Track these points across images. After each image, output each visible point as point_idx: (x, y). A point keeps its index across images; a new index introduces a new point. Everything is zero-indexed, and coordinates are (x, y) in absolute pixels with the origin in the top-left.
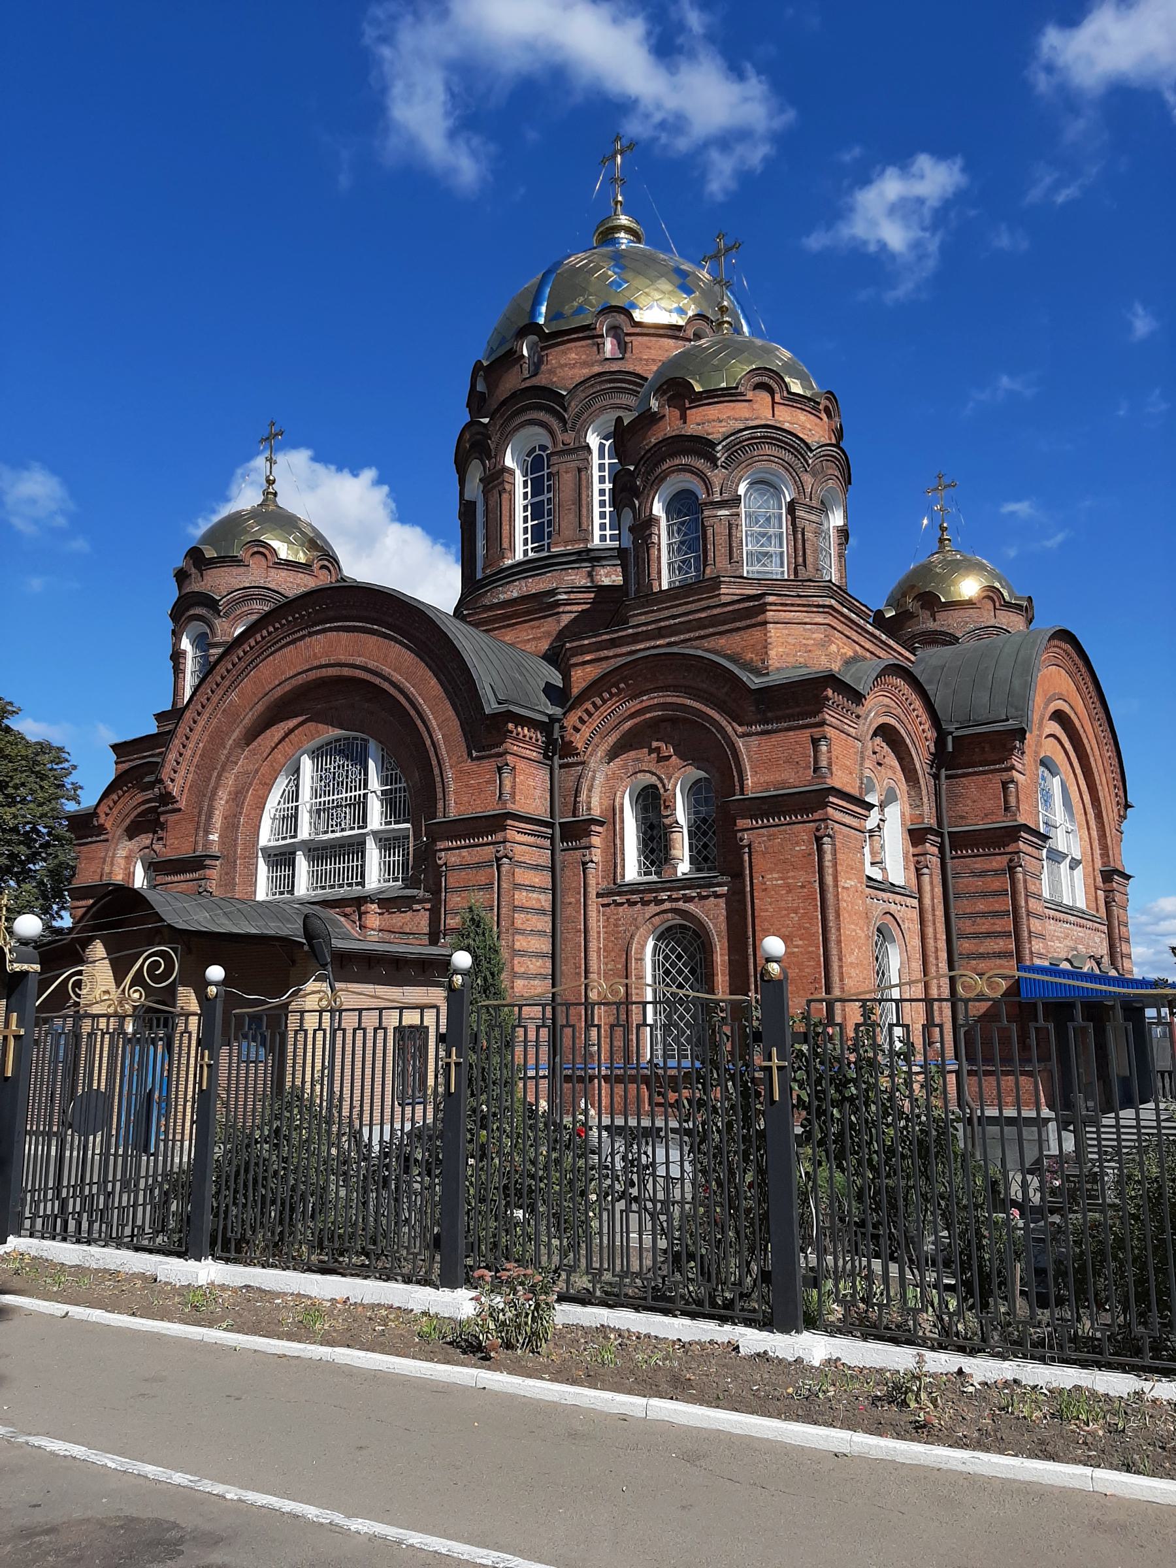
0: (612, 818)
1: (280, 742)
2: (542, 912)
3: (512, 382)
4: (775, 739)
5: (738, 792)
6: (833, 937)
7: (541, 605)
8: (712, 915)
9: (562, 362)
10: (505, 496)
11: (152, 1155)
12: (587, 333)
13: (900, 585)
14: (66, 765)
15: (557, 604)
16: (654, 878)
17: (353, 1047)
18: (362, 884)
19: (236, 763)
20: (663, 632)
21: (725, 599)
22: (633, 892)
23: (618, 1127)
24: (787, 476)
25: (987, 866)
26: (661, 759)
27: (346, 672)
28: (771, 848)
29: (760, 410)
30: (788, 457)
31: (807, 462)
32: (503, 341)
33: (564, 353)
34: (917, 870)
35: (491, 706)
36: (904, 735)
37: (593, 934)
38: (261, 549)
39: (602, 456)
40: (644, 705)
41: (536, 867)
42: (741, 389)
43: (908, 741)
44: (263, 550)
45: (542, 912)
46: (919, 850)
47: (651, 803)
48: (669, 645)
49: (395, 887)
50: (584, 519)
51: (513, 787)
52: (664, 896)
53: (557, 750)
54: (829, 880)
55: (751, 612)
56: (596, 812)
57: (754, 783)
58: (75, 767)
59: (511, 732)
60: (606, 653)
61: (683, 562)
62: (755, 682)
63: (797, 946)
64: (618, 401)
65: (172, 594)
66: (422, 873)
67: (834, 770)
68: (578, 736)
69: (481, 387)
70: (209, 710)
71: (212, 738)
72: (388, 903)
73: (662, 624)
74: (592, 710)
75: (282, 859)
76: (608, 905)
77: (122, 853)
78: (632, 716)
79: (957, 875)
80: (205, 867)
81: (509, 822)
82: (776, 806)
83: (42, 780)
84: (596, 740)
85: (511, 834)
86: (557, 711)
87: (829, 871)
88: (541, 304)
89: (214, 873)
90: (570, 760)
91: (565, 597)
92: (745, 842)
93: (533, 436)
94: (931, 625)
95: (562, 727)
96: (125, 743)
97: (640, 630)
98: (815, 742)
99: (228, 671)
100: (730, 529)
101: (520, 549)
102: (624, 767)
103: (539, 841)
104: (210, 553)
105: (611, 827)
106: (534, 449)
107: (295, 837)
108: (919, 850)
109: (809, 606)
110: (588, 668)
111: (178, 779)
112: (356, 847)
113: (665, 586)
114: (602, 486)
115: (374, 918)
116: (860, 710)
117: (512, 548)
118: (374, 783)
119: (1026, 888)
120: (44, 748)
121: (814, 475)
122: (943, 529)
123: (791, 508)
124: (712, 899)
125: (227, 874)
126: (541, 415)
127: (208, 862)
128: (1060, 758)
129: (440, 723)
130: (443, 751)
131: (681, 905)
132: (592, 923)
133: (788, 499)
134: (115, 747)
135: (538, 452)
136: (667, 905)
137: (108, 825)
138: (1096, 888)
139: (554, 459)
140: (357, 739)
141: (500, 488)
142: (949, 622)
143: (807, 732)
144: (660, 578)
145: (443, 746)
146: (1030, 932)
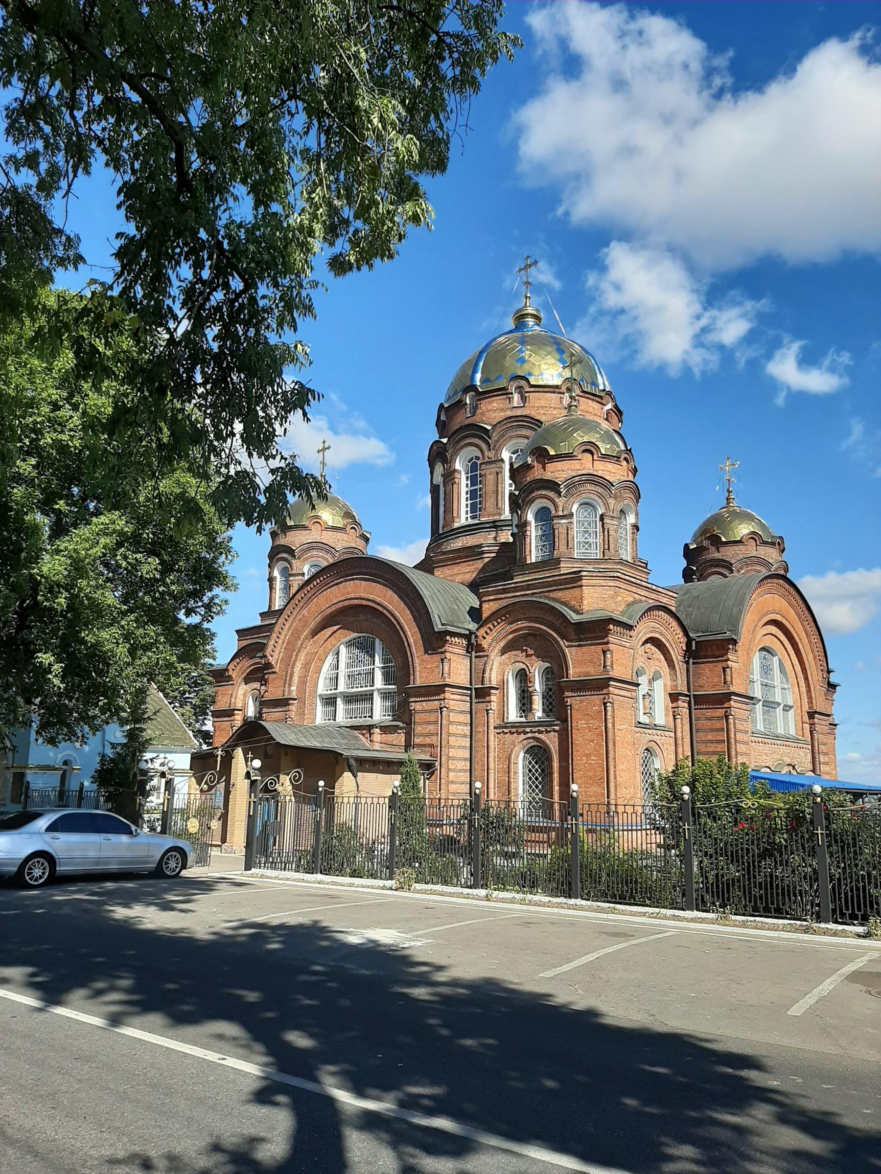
0: (502, 687)
2: (465, 736)
4: (585, 649)
6: (611, 756)
7: (473, 552)
8: (552, 740)
10: (455, 486)
12: (503, 391)
13: (700, 528)
15: (483, 553)
16: (523, 720)
17: (365, 799)
18: (371, 717)
21: (562, 572)
22: (513, 727)
24: (600, 501)
26: (527, 656)
27: (364, 602)
28: (581, 706)
29: (585, 464)
30: (600, 490)
32: (456, 393)
33: (490, 403)
34: (674, 716)
35: (438, 627)
36: (665, 642)
37: (492, 749)
41: (461, 712)
43: (667, 645)
44: (317, 520)
45: (465, 736)
46: (675, 705)
47: (523, 677)
49: (387, 720)
50: (499, 502)
51: (449, 670)
52: (528, 730)
53: (474, 648)
54: (610, 725)
55: (575, 580)
56: (494, 683)
57: (574, 672)
61: (543, 546)
62: (574, 617)
66: (402, 714)
67: (614, 667)
69: (443, 418)
70: (291, 618)
71: (293, 634)
72: (386, 729)
74: (492, 627)
75: (330, 701)
79: (697, 719)
80: (289, 705)
84: (494, 644)
85: (447, 695)
86: (473, 626)
87: (610, 721)
93: (471, 452)
94: (717, 555)
95: (476, 636)
98: (604, 652)
102: (509, 658)
103: (463, 698)
106: (472, 459)
107: (336, 689)
110: (492, 603)
111: (275, 654)
112: (368, 697)
113: (533, 561)
116: (632, 633)
117: (459, 516)
119: (735, 727)
121: (615, 499)
122: (729, 492)
126: (476, 441)
127: (290, 702)
128: (776, 646)
131: (537, 735)
132: (491, 743)
134: (237, 631)
136: (530, 735)
137: (234, 676)
138: (803, 723)
139: (483, 467)
142: (728, 554)
146: (736, 752)
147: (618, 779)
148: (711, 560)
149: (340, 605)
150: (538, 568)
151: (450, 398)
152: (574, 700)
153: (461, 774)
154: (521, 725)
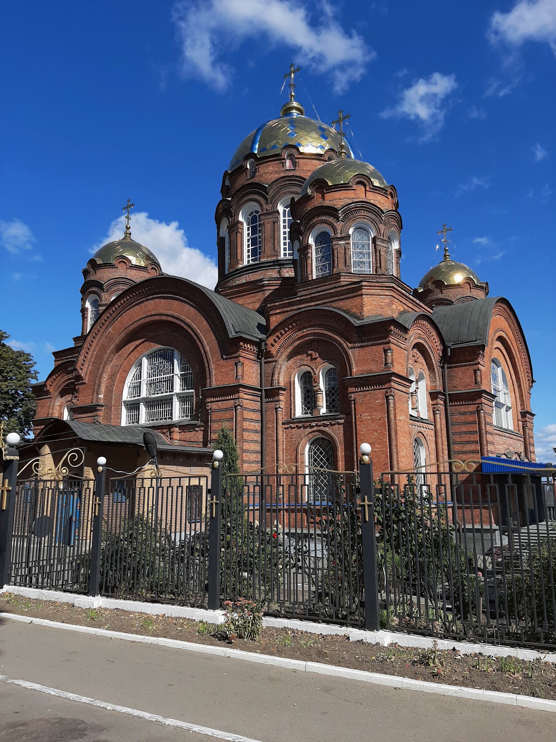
0: (289, 387)
1: (132, 351)
2: (256, 431)
3: (242, 181)
4: (367, 350)
5: (349, 375)
6: (394, 443)
7: (256, 286)
8: (337, 433)
9: (266, 171)
10: (239, 235)
11: (72, 546)
12: (278, 157)
14: (31, 362)
15: (263, 286)
16: (309, 415)
18: (171, 418)
19: (112, 361)
20: (314, 299)
21: (343, 283)
22: (299, 422)
23: (292, 533)
24: (372, 225)
25: (467, 410)
26: (312, 359)
27: (164, 318)
28: (364, 402)
29: (359, 194)
30: (373, 216)
31: (381, 219)
32: (238, 161)
33: (267, 167)
34: (434, 412)
35: (232, 334)
36: (428, 348)
37: (280, 442)
38: (124, 260)
39: (284, 216)
40: (305, 333)
41: (253, 410)
42: (350, 184)
43: (429, 351)
44: (124, 260)
45: (256, 431)
46: (434, 402)
47: (308, 380)
48: (316, 305)
49: (187, 420)
50: (276, 246)
51: (243, 372)
52: (314, 424)
53: (263, 355)
54: (392, 416)
55: (355, 290)
56: (282, 385)
57: (356, 370)
58: (35, 363)
59: (242, 346)
60: (286, 309)
61: (323, 266)
62: (357, 323)
63: (377, 448)
64: (292, 190)
65: (81, 281)
66: (200, 413)
67: (394, 364)
68: (273, 348)
69: (227, 183)
70: (99, 336)
71: (100, 349)
72: (183, 427)
73: (313, 295)
74: (280, 336)
75: (133, 406)
76: (287, 428)
77: (57, 403)
78: (299, 339)
79: (452, 414)
80: (97, 410)
81: (241, 389)
82: (367, 382)
83: (20, 369)
84: (282, 350)
85: (242, 395)
86: (263, 336)
87: (392, 412)
88: (256, 144)
89: (101, 413)
90: (270, 360)
91: (267, 282)
92: (352, 399)
94: (440, 296)
95: (266, 344)
96: (59, 351)
97: (303, 298)
98: (385, 351)
99: (108, 318)
100: (345, 251)
101: (246, 260)
102: (295, 363)
103: (255, 398)
104: (99, 262)
105: (289, 391)
107: (139, 396)
108: (434, 402)
109: (383, 287)
110: (278, 316)
111: (84, 368)
112: (168, 401)
113: (314, 278)
114: (285, 230)
115: (177, 434)
116: (407, 336)
117: (242, 259)
118: (177, 371)
119: (485, 420)
120: (21, 354)
121: (385, 225)
123: (374, 240)
124: (337, 425)
125: (107, 413)
126: (256, 197)
127: (98, 408)
128: (501, 359)
129: (208, 342)
130: (210, 355)
132: (280, 437)
133: (373, 236)
134: (55, 354)
135: (254, 214)
136: (315, 428)
137: (51, 391)
138: (518, 420)
139: (262, 217)
140: (169, 350)
141: (237, 231)
143: (382, 347)
144: (312, 273)
145: (209, 353)
146: (487, 441)
147: (400, 464)
148: (436, 300)
149: (142, 322)
150: (320, 283)
151: (233, 166)
152: (357, 395)
153: (254, 465)
154: (307, 420)
